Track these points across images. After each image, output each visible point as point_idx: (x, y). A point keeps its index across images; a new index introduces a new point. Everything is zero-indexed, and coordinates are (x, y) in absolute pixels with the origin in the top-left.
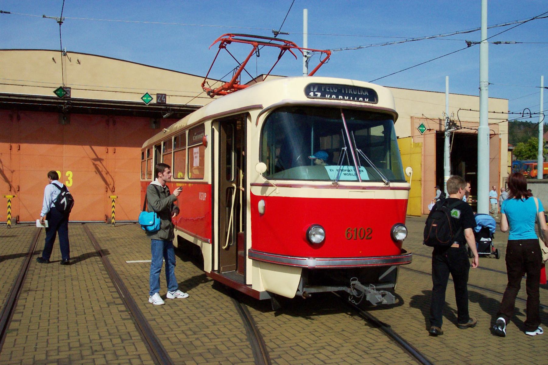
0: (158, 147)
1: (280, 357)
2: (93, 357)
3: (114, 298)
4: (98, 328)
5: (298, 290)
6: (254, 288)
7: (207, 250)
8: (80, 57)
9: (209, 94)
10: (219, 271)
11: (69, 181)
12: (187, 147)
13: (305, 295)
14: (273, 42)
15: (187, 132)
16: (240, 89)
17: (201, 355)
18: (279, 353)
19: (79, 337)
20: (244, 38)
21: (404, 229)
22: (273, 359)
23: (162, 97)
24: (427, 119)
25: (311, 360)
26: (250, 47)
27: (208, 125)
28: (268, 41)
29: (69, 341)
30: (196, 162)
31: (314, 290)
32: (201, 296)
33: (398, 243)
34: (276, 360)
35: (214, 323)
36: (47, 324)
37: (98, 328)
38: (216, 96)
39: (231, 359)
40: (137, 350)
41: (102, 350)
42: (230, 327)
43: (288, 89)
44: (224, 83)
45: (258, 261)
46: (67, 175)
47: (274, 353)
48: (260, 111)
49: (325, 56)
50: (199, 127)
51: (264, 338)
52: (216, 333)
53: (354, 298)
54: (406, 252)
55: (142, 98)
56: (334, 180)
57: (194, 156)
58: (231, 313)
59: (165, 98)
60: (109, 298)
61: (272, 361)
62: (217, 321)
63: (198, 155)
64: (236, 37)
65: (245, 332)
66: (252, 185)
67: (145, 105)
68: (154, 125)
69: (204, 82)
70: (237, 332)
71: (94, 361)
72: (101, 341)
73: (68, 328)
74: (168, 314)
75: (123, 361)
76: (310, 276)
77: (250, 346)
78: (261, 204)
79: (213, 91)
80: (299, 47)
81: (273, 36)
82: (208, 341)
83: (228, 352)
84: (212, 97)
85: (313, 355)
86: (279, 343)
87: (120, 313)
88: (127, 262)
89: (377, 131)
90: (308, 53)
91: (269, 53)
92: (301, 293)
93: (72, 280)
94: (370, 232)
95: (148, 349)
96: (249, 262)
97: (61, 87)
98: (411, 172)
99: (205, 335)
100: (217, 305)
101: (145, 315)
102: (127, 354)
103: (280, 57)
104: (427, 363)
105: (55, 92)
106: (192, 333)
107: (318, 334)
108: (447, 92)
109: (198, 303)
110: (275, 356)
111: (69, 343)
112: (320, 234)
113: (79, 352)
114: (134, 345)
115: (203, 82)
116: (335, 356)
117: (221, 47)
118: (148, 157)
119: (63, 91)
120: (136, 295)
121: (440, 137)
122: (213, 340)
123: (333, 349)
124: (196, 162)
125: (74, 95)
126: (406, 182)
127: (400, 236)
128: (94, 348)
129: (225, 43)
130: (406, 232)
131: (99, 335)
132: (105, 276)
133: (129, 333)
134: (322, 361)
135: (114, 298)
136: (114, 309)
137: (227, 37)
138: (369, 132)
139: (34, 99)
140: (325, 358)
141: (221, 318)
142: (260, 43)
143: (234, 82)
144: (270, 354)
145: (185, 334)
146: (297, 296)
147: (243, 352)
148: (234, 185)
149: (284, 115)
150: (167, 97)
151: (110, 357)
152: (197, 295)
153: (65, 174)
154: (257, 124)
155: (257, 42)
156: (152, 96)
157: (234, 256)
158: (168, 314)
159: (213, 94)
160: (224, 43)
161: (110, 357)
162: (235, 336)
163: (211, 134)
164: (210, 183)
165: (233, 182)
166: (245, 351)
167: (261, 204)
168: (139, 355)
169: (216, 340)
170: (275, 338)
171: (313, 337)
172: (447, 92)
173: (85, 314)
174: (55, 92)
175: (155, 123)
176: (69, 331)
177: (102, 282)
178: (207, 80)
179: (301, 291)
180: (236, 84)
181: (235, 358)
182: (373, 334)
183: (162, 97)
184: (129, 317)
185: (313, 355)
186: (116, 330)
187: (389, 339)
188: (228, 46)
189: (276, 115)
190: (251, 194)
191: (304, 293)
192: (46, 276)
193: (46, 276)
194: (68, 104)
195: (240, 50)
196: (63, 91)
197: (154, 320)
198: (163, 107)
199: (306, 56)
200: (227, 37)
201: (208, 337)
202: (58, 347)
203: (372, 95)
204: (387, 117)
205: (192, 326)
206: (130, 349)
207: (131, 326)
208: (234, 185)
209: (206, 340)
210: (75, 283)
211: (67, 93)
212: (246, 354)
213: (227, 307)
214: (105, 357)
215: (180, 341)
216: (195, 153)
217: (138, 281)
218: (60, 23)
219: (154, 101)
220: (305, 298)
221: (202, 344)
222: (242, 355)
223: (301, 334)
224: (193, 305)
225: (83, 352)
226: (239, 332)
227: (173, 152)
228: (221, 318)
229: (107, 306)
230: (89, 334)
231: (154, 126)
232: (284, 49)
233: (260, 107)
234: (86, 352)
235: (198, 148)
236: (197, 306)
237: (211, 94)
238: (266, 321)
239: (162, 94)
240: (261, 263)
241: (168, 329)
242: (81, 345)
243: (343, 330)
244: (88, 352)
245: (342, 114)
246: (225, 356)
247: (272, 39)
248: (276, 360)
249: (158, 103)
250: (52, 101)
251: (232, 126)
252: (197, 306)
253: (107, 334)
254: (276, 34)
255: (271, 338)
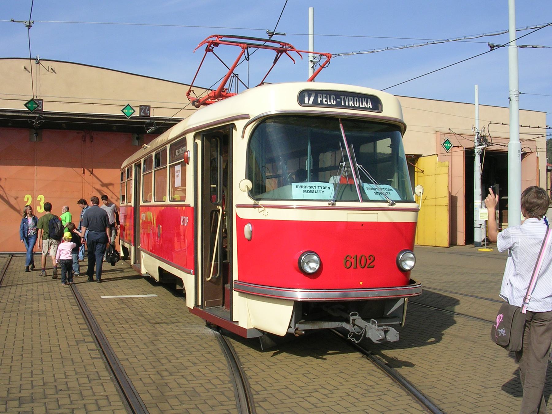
0: (138, 166)
1: (265, 400)
2: (57, 396)
3: (84, 336)
4: (64, 367)
5: (290, 327)
6: (240, 325)
7: (189, 282)
8: (54, 65)
9: (194, 104)
10: (202, 306)
11: (41, 206)
12: (168, 165)
13: (297, 331)
14: (268, 44)
15: (168, 146)
16: (226, 97)
17: (176, 397)
18: (264, 396)
19: (43, 376)
20: (233, 40)
21: (412, 256)
22: (257, 403)
23: (145, 109)
24: (455, 134)
25: (300, 403)
26: (239, 49)
27: (190, 137)
28: (261, 43)
29: (32, 379)
30: (178, 183)
31: (308, 327)
32: (183, 334)
33: (406, 273)
34: (261, 403)
35: (195, 364)
36: (10, 361)
37: (64, 367)
38: (201, 106)
39: (209, 402)
40: (105, 391)
41: (66, 389)
42: (212, 368)
43: (279, 97)
44: (210, 91)
45: (244, 293)
46: (38, 199)
47: (258, 396)
48: (246, 121)
49: (324, 59)
50: (180, 142)
51: (250, 380)
52: (195, 374)
53: (355, 336)
54: (415, 282)
55: (122, 111)
56: (331, 200)
57: (176, 174)
58: (215, 353)
59: (149, 110)
60: (79, 336)
61: (256, 405)
62: (198, 361)
63: (180, 174)
64: (224, 39)
65: (228, 373)
66: (238, 206)
67: (126, 118)
68: (137, 141)
69: (190, 91)
70: (219, 374)
71: (58, 401)
72: (66, 380)
73: (32, 366)
74: (143, 354)
75: (89, 402)
76: (303, 311)
77: (232, 388)
78: (248, 228)
79: (198, 101)
80: (297, 49)
81: (267, 37)
82: (186, 382)
83: (206, 394)
84: (198, 107)
85: (303, 398)
86: (265, 384)
87: (90, 352)
88: (102, 297)
89: (384, 146)
90: (315, 58)
91: (262, 58)
92: (292, 331)
93: (39, 315)
94: (372, 259)
95: (117, 390)
96: (235, 294)
97: (32, 100)
98: (421, 191)
99: (182, 376)
100: (200, 345)
101: (117, 354)
102: (94, 394)
103: (275, 62)
104: (437, 411)
105: (25, 105)
106: (167, 374)
107: (310, 376)
108: (477, 104)
109: (179, 342)
110: (260, 400)
111: (32, 381)
112: (315, 261)
113: (42, 390)
114: (103, 385)
115: (188, 90)
116: (328, 400)
117: (208, 50)
118: (127, 178)
119: (35, 104)
120: (109, 332)
121: (469, 155)
122: (191, 382)
123: (326, 392)
124: (178, 183)
125: (47, 108)
126: (415, 202)
127: (408, 264)
128: (59, 388)
129: (212, 46)
130: (414, 259)
131: (97, 404)
132: (76, 312)
133: (97, 372)
134: (313, 404)
135: (84, 336)
136: (83, 348)
137: (215, 39)
138: (375, 147)
139: (4, 114)
140: (316, 401)
141: (202, 359)
142: (249, 46)
143: (222, 89)
144: (254, 396)
145: (161, 375)
146: (288, 334)
147: (224, 395)
148: (220, 208)
149: (270, 123)
150: (152, 109)
151: (75, 397)
152: (178, 334)
153: (37, 198)
154: (243, 137)
155: (247, 45)
156: (134, 108)
157: (218, 289)
158: (143, 354)
159: (199, 103)
160: (211, 46)
161: (75, 397)
162: (217, 377)
163: (193, 146)
164: (192, 205)
165: (218, 204)
166: (226, 393)
167: (248, 228)
168: (107, 396)
169: (194, 382)
170: (262, 380)
171: (305, 380)
172: (477, 104)
173: (51, 351)
174: (25, 105)
175: (138, 139)
176: (32, 369)
177: (72, 319)
178: (192, 88)
179: (293, 327)
180: (224, 92)
181: (215, 401)
182: (375, 376)
183: (145, 109)
184: (99, 356)
185: (303, 398)
186: (83, 370)
187: (391, 381)
188: (215, 49)
189: (263, 123)
190: (237, 217)
191: (297, 329)
192: (11, 311)
193: (11, 311)
194: (39, 118)
195: (229, 53)
196: (35, 104)
197: (127, 359)
198: (147, 121)
199: (312, 61)
200: (215, 39)
201: (186, 379)
202: (21, 385)
203: (376, 103)
204: (394, 128)
205: (169, 366)
206: (98, 389)
207: (100, 364)
208: (220, 208)
209: (183, 381)
210: (43, 318)
211: (38, 106)
212: (228, 398)
213: (211, 346)
214: (70, 397)
215: (154, 383)
216: (177, 171)
217: (113, 318)
218: (29, 27)
219: (137, 114)
220: (297, 335)
221: (178, 386)
222: (222, 398)
223: (292, 376)
224: (173, 345)
225: (46, 390)
226: (222, 374)
227: (153, 171)
228: (202, 359)
229: (75, 344)
230: (54, 372)
231: (136, 143)
232: (280, 51)
233: (246, 117)
234: (50, 391)
235: (180, 165)
236: (177, 345)
237: (197, 104)
238: (253, 360)
239: (146, 106)
240: (248, 295)
241: (142, 369)
242: (44, 384)
243: (341, 372)
244: (52, 391)
245: (341, 125)
246: (204, 398)
247: (266, 41)
248: (261, 403)
249: (140, 116)
250: (23, 115)
251: (217, 138)
252: (177, 345)
253: (74, 373)
254: (271, 34)
255: (257, 380)
